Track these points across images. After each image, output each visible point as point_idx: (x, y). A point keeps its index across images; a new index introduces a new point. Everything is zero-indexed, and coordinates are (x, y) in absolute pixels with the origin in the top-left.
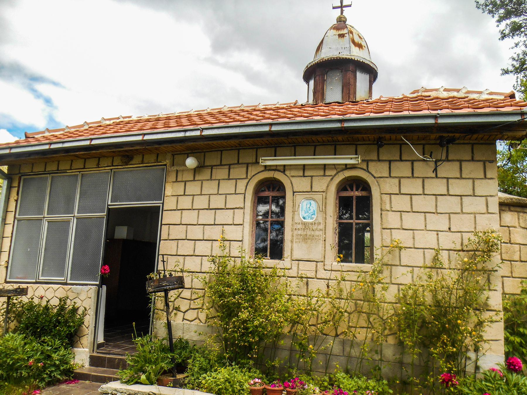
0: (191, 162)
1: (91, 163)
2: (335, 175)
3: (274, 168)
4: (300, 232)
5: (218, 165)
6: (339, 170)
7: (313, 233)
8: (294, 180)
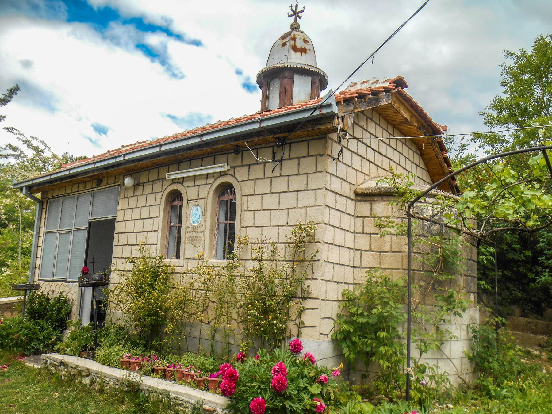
0: (128, 181)
1: (81, 188)
2: (213, 182)
3: (177, 181)
4: (190, 235)
5: (147, 182)
6: (216, 178)
7: (197, 235)
8: (188, 189)
